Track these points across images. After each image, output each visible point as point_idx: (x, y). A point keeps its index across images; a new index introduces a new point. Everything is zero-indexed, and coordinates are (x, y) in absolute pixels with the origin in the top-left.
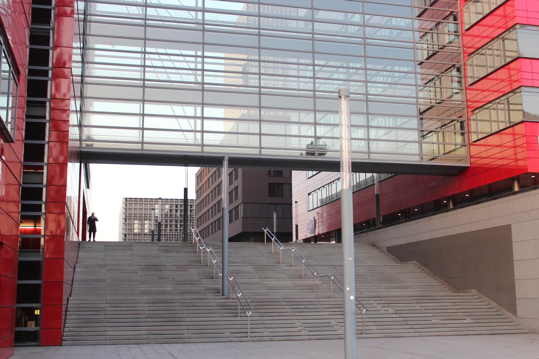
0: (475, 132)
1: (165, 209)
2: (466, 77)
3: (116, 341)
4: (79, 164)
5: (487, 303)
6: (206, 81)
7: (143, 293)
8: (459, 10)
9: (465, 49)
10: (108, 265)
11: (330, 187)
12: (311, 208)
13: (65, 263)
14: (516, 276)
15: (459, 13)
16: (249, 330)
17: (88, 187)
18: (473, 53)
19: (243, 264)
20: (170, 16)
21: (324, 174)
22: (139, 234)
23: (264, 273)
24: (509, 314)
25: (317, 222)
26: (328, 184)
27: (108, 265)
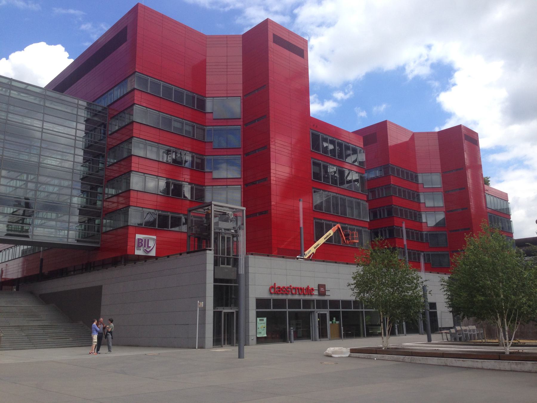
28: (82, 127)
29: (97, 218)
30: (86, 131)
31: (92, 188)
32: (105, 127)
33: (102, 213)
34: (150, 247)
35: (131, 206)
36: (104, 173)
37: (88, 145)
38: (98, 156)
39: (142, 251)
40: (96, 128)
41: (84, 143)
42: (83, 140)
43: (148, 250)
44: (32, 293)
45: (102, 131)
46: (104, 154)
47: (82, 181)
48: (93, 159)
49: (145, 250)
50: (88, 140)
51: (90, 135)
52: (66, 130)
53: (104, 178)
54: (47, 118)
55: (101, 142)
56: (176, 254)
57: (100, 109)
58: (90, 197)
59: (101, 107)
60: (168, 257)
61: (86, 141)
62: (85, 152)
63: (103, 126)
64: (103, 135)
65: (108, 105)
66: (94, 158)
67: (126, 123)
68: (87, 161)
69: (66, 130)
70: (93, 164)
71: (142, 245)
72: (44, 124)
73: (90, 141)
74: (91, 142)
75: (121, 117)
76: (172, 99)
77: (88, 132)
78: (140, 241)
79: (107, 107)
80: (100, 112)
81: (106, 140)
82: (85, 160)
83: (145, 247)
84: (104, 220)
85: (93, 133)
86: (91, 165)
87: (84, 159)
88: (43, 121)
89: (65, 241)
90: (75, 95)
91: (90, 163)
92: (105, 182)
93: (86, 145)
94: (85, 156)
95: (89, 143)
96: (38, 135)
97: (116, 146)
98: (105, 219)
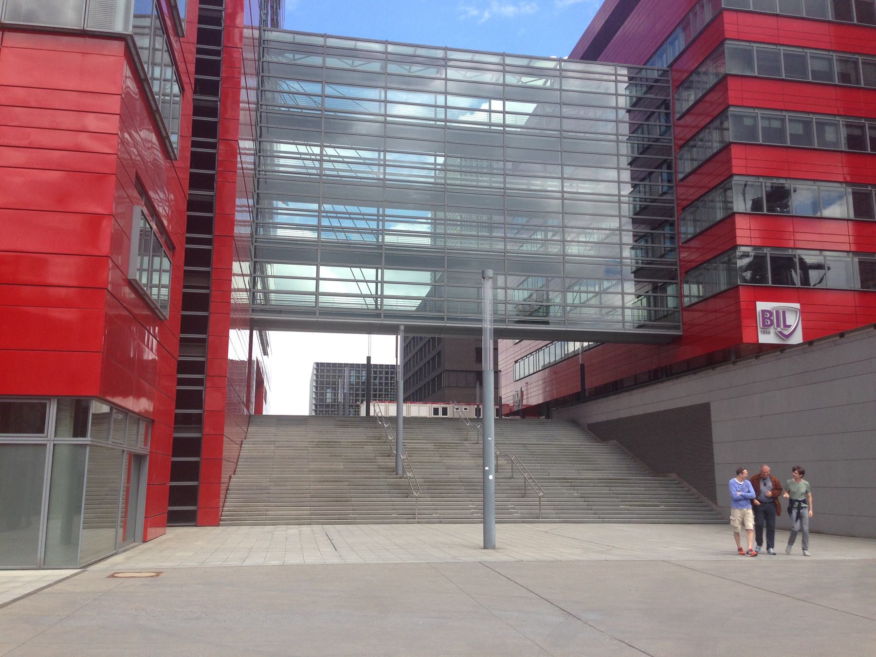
0: (687, 296)
1: (362, 376)
2: (679, 233)
3: (275, 522)
4: (248, 332)
5: (687, 489)
6: (322, 289)
7: (312, 471)
8: (673, 158)
9: (679, 201)
10: (278, 441)
11: (537, 354)
12: (518, 378)
13: (225, 439)
14: (716, 460)
15: (674, 161)
16: (417, 512)
17: (265, 353)
18: (688, 206)
19: (425, 441)
20: (349, 169)
21: (526, 343)
22: (332, 405)
23: (445, 451)
24: (711, 503)
25: (525, 393)
26: (536, 351)
27: (278, 441)
28: (626, 176)
29: (672, 281)
30: (634, 182)
31: (655, 289)
32: (667, 108)
33: (679, 271)
34: (790, 326)
35: (736, 175)
36: (678, 257)
37: (640, 207)
38: (660, 225)
39: (772, 335)
40: (651, 173)
41: (631, 206)
42: (629, 200)
43: (786, 333)
44: (575, 423)
45: (665, 176)
46: (676, 269)
47: (631, 167)
48: (652, 234)
49: (780, 332)
50: (640, 198)
51: (642, 189)
52: (602, 188)
53: (675, 205)
54: (568, 171)
55: (664, 198)
56: (867, 327)
57: (655, 75)
58: (651, 195)
59: (656, 71)
60: (842, 335)
61: (634, 201)
62: (634, 221)
63: (665, 166)
64: (667, 184)
65: (669, 64)
66: (653, 230)
67: (715, 151)
68: (641, 237)
69: (602, 188)
70: (652, 243)
71: (772, 322)
72: (565, 184)
73: (642, 139)
74: (645, 202)
75: (702, 140)
76: (833, 81)
77: (638, 183)
78: (767, 315)
79: (668, 69)
80: (657, 81)
81: (675, 192)
82: (637, 237)
83: (778, 326)
84: (685, 285)
85: (647, 182)
86: (650, 245)
87: (634, 236)
88: (562, 178)
89: (617, 328)
90: (609, 60)
91: (647, 242)
92: (677, 211)
93: (635, 208)
94: (632, 120)
95: (641, 203)
96: (555, 204)
97: (697, 200)
98: (687, 282)
